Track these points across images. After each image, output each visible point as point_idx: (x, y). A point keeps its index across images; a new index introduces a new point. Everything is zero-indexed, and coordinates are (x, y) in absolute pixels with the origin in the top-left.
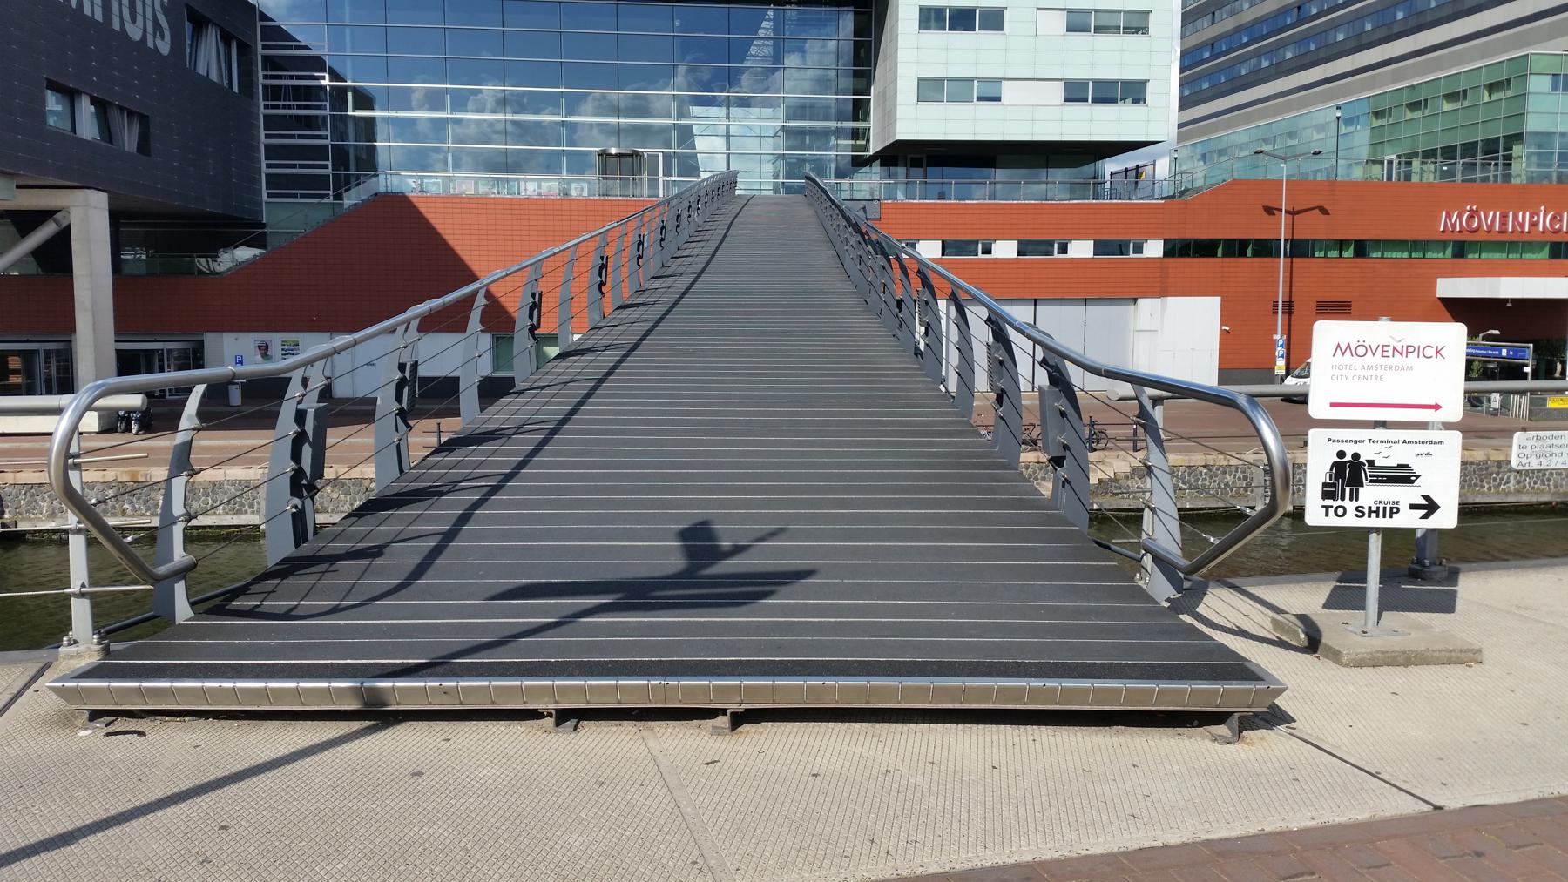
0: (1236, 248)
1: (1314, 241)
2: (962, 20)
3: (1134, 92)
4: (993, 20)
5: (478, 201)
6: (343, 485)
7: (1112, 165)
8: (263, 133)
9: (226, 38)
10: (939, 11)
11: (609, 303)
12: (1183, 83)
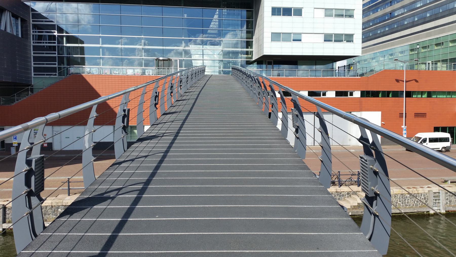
0: (386, 94)
2: (287, 12)
3: (349, 38)
4: (298, 12)
5: (111, 77)
7: (339, 64)
8: (32, 52)
9: (15, 16)
10: (279, 9)
12: (363, 34)
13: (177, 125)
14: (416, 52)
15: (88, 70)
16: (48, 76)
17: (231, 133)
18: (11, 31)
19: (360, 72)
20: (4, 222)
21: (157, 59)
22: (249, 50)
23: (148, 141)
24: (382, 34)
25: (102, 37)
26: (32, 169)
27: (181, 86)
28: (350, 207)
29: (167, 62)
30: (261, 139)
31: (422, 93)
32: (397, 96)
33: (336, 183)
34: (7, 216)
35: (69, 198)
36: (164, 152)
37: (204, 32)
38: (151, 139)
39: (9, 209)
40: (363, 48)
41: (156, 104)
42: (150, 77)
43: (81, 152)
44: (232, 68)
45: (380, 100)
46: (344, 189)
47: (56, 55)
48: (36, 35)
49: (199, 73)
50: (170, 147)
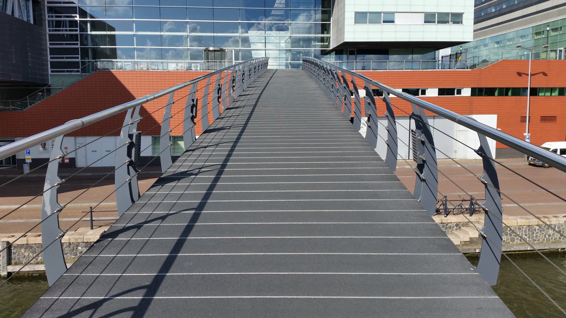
0: (504, 92)
1: (539, 88)
3: (457, 18)
5: (147, 73)
6: (31, 247)
7: (446, 52)
8: (48, 43)
11: (200, 127)
12: (476, 12)
13: (224, 150)
14: (543, 36)
15: (119, 64)
16: (68, 73)
17: (307, 166)
18: (19, 16)
19: (469, 63)
20: (9, 263)
21: (207, 49)
22: (325, 35)
23: (173, 184)
24: (497, 14)
25: (136, 22)
26: (133, 142)
27: (234, 86)
28: (459, 243)
29: (219, 53)
30: (357, 178)
31: (552, 90)
32: (519, 95)
33: (441, 211)
34: (13, 256)
35: (91, 232)
36: (196, 206)
37: (266, 14)
38: (179, 179)
39: (15, 247)
40: (474, 31)
41: (193, 118)
42: (197, 72)
43: (112, 169)
44: (303, 60)
45: (495, 99)
46: (452, 219)
47: (79, 46)
48: (53, 21)
49: (260, 67)
50: (207, 196)
